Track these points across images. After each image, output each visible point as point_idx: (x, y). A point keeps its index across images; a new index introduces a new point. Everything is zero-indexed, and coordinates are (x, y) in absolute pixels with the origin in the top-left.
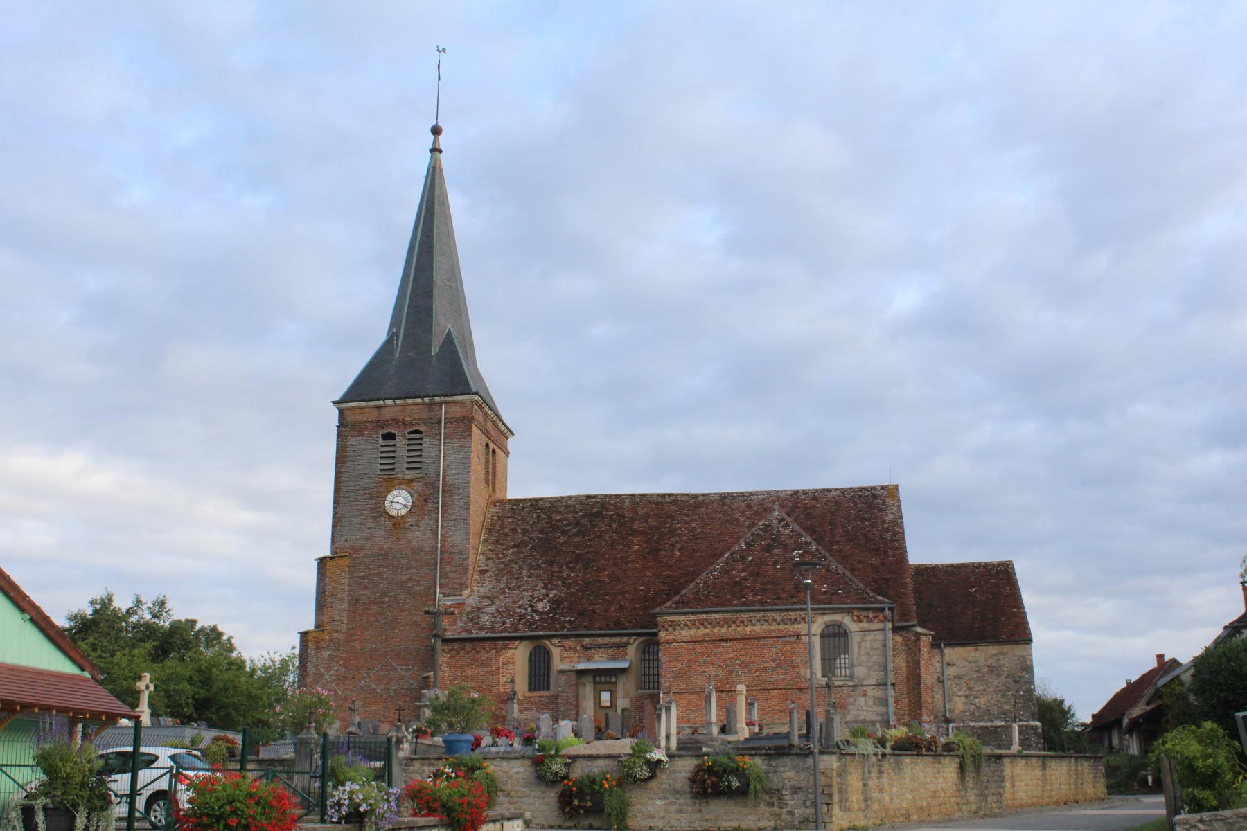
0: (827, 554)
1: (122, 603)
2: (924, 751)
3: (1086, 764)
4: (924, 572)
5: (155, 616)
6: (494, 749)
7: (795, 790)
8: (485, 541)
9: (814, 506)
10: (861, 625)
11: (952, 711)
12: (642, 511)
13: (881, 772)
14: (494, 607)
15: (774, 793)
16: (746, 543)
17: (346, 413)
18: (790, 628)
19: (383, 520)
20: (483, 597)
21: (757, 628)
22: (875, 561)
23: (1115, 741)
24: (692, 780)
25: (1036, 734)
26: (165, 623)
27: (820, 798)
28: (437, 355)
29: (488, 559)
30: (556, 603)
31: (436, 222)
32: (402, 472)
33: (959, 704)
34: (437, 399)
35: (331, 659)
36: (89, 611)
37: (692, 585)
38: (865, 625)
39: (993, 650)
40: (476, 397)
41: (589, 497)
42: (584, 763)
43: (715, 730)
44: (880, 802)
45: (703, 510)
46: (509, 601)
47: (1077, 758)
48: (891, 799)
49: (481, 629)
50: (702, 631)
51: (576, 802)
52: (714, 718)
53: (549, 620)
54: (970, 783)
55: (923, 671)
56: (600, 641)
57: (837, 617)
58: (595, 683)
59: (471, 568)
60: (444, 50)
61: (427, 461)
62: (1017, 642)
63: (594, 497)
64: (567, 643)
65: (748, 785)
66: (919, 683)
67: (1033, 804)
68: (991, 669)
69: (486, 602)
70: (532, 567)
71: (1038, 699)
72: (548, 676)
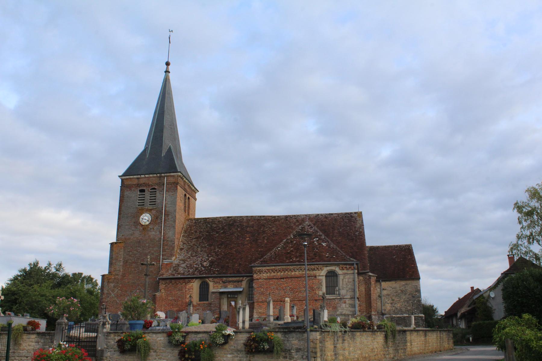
0: (329, 240)
1: (42, 265)
2: (366, 329)
3: (444, 334)
4: (373, 249)
5: (57, 270)
6: (158, 328)
7: (298, 350)
8: (183, 236)
9: (325, 221)
10: (343, 271)
11: (385, 310)
12: (251, 223)
13: (344, 340)
14: (185, 264)
15: (287, 352)
16: (293, 235)
17: (124, 181)
18: (312, 273)
19: (138, 227)
20: (180, 260)
21: (297, 273)
22: (351, 244)
23: (455, 322)
24: (245, 345)
25: (422, 320)
26: (61, 274)
27: (309, 353)
28: (164, 156)
29: (184, 244)
30: (212, 263)
31: (166, 101)
32: (148, 206)
33: (388, 307)
34: (163, 175)
35: (114, 287)
36: (28, 268)
37: (269, 254)
38: (345, 271)
39: (403, 283)
40: (180, 174)
41: (228, 217)
42: (193, 335)
43: (272, 319)
44: (343, 355)
45: (277, 223)
46: (191, 261)
47: (440, 331)
48: (349, 353)
49: (179, 274)
50: (273, 274)
51: (187, 356)
52: (271, 313)
53: (209, 270)
54: (390, 344)
55: (372, 292)
56: (231, 279)
57: (333, 268)
58: (228, 298)
59: (176, 248)
60: (172, 31)
61: (158, 201)
62: (413, 279)
63: (231, 217)
64: (216, 280)
65: (273, 347)
66: (370, 298)
67: (421, 353)
68: (402, 291)
69: (182, 262)
70: (202, 247)
71: (423, 305)
72: (208, 295)
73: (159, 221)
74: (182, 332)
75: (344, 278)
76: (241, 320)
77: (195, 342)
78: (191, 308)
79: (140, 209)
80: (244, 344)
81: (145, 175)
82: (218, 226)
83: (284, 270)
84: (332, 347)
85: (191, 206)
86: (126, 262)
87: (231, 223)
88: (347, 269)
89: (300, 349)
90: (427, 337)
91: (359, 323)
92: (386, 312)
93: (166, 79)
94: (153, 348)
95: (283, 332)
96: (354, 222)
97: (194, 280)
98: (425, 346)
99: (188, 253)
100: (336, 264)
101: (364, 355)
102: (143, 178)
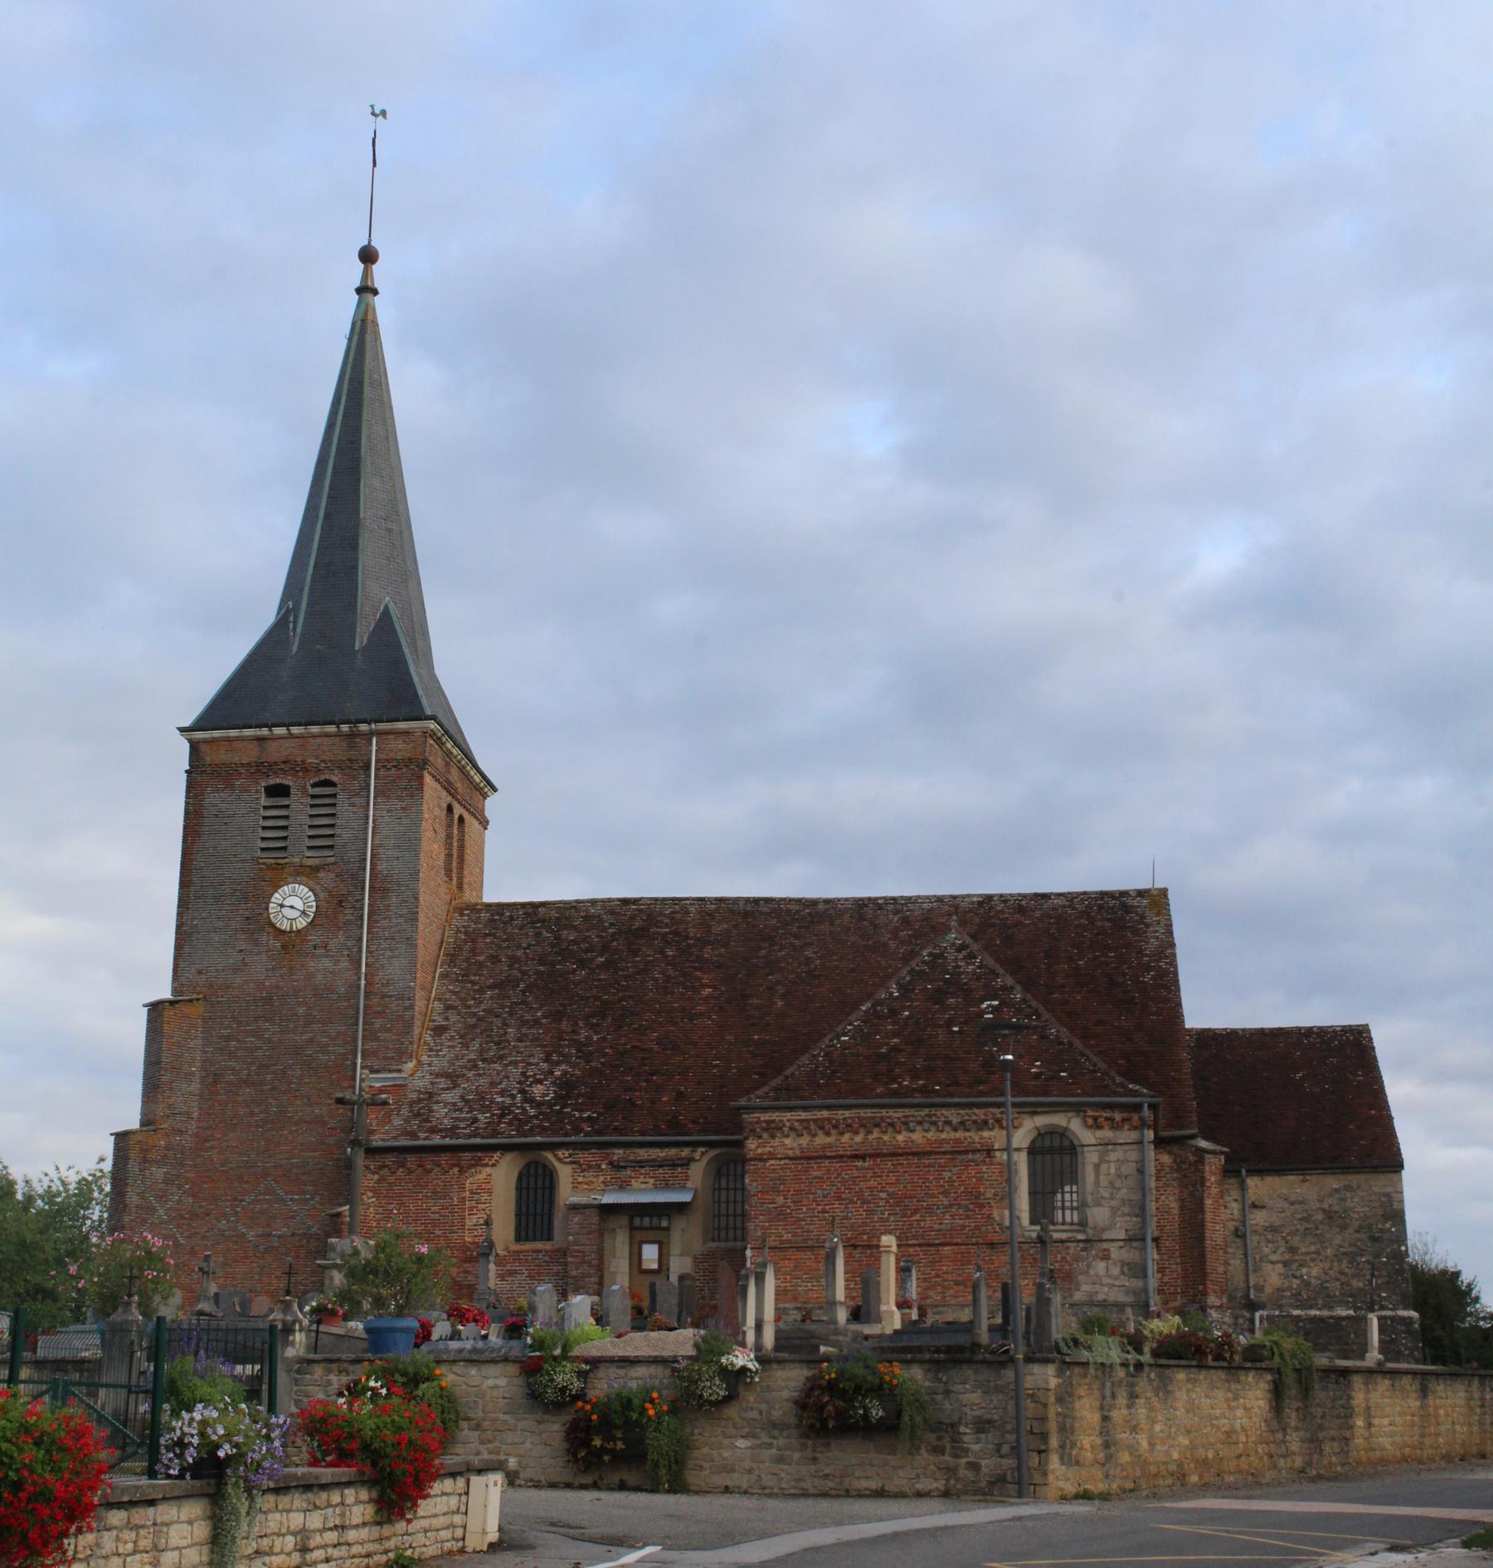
0: (1041, 1009)
4: (1209, 1039)
9: (1019, 924)
10: (1099, 1133)
13: (1133, 1396)
14: (457, 1092)
16: (900, 987)
17: (203, 747)
18: (975, 1137)
20: (437, 1075)
21: (917, 1136)
24: (801, 1404)
25: (1410, 1332)
28: (364, 649)
29: (448, 1008)
30: (566, 1088)
33: (1273, 1277)
34: (363, 727)
37: (804, 1060)
38: (1107, 1134)
39: (1333, 1182)
40: (432, 725)
41: (625, 902)
42: (613, 1371)
43: (842, 1315)
44: (1132, 1449)
45: (824, 927)
49: (434, 1130)
50: (821, 1139)
51: (597, 1442)
52: (840, 1295)
55: (1209, 1216)
56: (643, 1154)
57: (1058, 1120)
58: (632, 1228)
60: (383, 113)
61: (344, 835)
62: (1375, 1169)
63: (636, 901)
64: (584, 1156)
65: (899, 1414)
66: (1201, 1238)
67: (1405, 1459)
68: (1330, 1215)
69: (443, 1083)
70: (524, 1023)
71: (1414, 1268)
72: (551, 1215)
73: (348, 914)
74: (576, 1359)
75: (1102, 1161)
76: (751, 1321)
77: (625, 1393)
78: (492, 1266)
79: (269, 867)
80: (796, 1402)
81: (288, 725)
82: (585, 939)
83: (867, 1126)
84: (1094, 1418)
85: (468, 851)
86: (215, 1082)
87: (637, 924)
88: (1116, 1127)
89: (989, 1422)
90: (1430, 1400)
91: (1182, 1336)
92: (1263, 1298)
93: (364, 321)
94: (471, 1415)
95: (930, 1361)
96: (1136, 932)
97: (496, 1156)
98: (1423, 1435)
99: (466, 1046)
100: (1069, 1104)
101: (1201, 1452)
102: (281, 738)
